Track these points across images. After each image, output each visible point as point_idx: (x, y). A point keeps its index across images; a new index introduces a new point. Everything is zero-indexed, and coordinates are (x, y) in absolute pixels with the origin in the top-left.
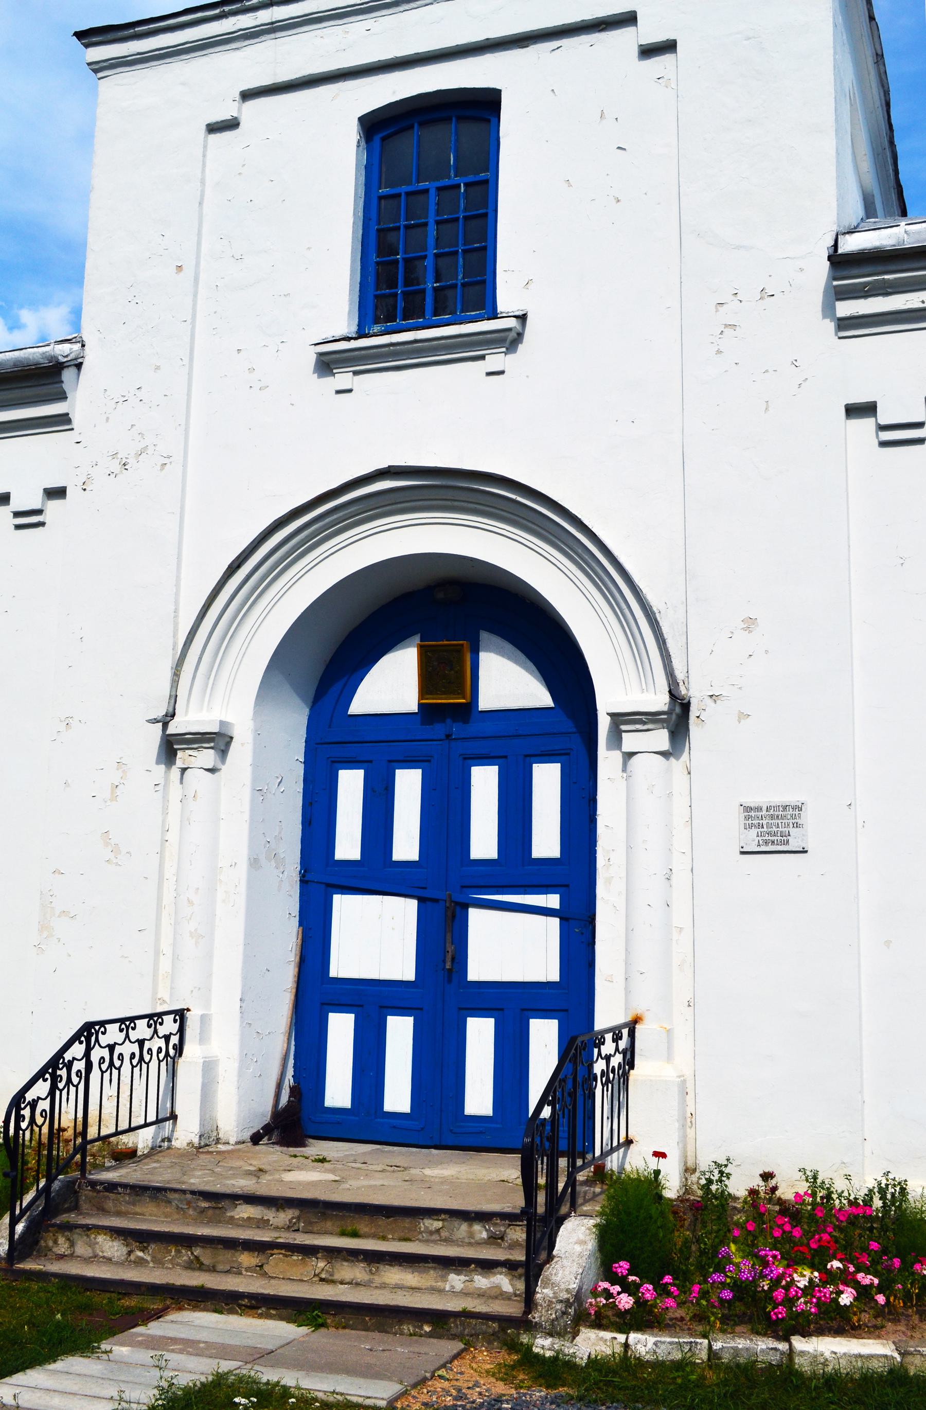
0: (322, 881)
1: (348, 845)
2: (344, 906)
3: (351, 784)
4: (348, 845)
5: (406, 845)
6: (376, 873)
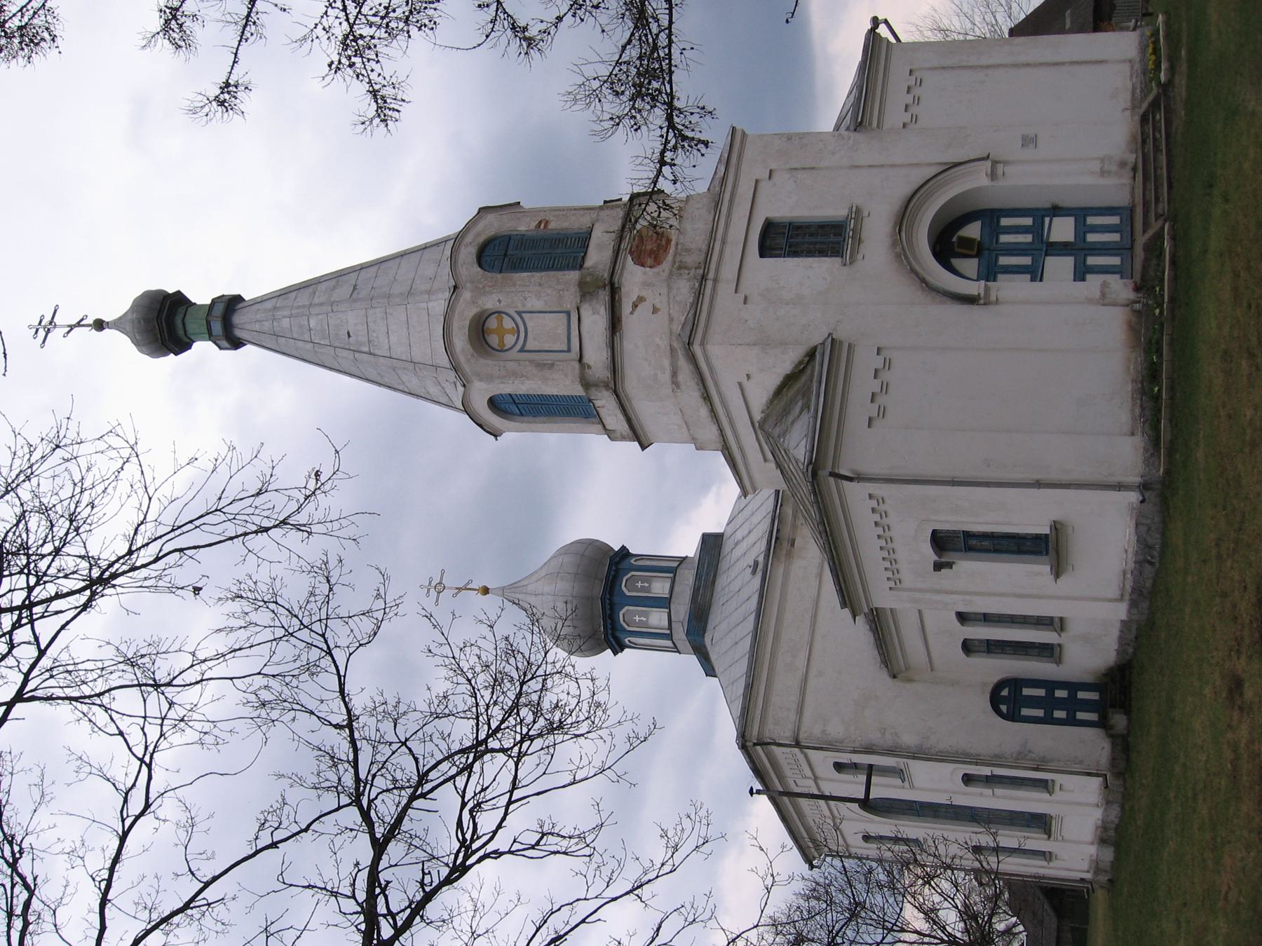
0: (1080, 214)
1: (1091, 220)
2: (1070, 221)
3: (1115, 220)
4: (1091, 220)
5: (1091, 238)
6: (1082, 229)
